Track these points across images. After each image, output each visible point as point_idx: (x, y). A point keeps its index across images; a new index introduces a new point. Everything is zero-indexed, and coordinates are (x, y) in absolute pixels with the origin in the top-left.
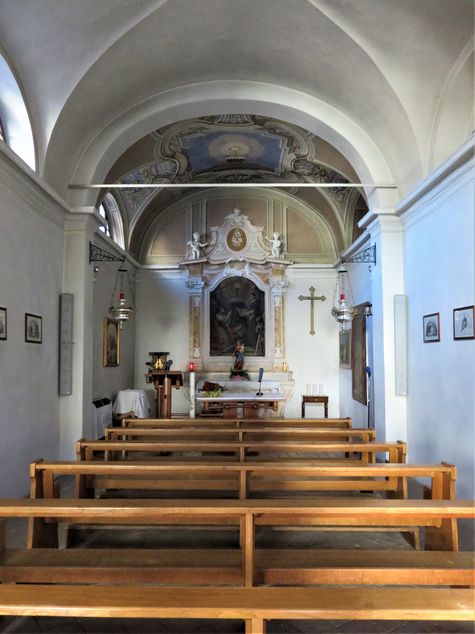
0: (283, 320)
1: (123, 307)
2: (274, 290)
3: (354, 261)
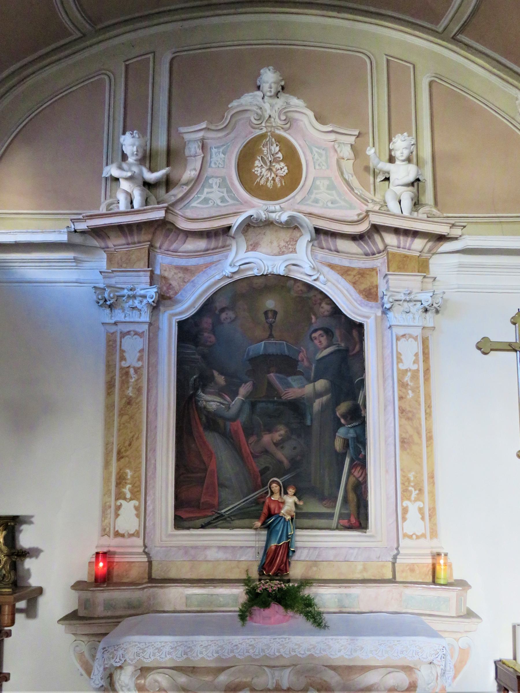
0: (428, 414)
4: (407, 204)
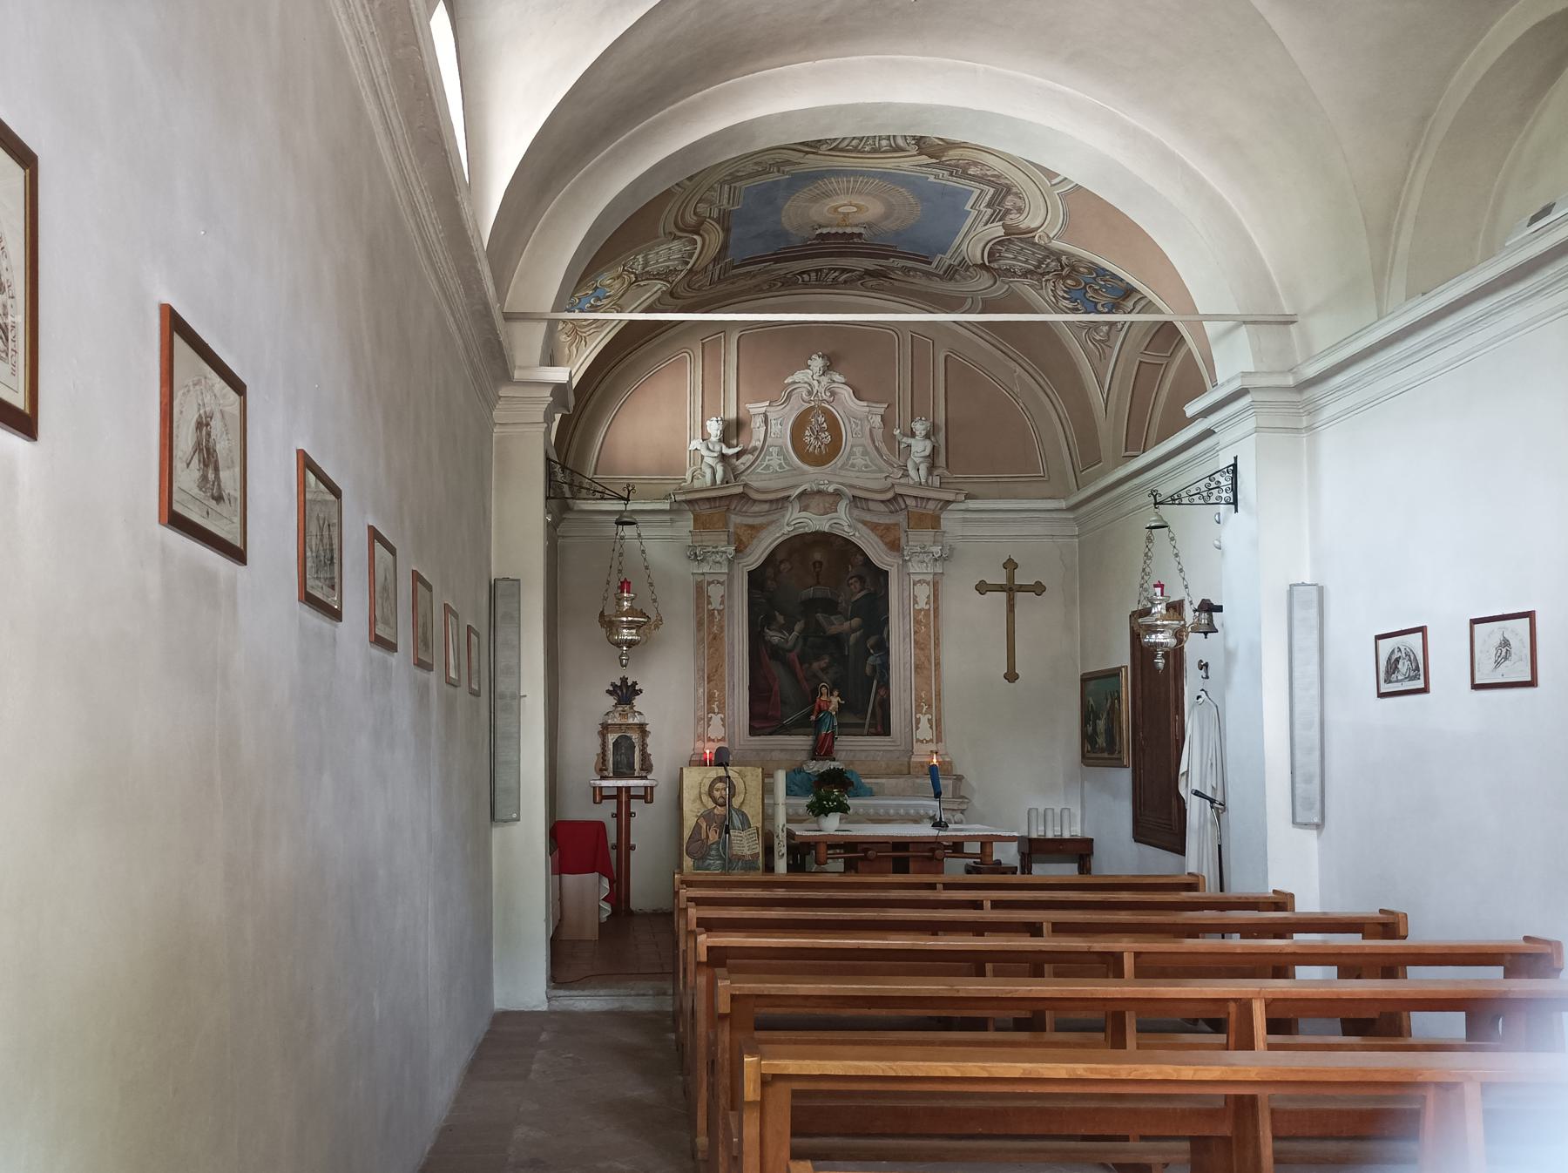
0: (937, 645)
1: (626, 614)
2: (914, 567)
3: (1185, 501)
4: (923, 472)
